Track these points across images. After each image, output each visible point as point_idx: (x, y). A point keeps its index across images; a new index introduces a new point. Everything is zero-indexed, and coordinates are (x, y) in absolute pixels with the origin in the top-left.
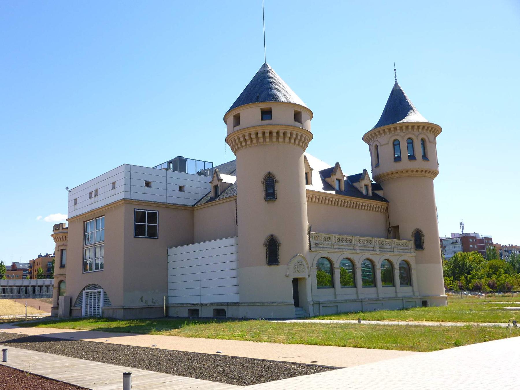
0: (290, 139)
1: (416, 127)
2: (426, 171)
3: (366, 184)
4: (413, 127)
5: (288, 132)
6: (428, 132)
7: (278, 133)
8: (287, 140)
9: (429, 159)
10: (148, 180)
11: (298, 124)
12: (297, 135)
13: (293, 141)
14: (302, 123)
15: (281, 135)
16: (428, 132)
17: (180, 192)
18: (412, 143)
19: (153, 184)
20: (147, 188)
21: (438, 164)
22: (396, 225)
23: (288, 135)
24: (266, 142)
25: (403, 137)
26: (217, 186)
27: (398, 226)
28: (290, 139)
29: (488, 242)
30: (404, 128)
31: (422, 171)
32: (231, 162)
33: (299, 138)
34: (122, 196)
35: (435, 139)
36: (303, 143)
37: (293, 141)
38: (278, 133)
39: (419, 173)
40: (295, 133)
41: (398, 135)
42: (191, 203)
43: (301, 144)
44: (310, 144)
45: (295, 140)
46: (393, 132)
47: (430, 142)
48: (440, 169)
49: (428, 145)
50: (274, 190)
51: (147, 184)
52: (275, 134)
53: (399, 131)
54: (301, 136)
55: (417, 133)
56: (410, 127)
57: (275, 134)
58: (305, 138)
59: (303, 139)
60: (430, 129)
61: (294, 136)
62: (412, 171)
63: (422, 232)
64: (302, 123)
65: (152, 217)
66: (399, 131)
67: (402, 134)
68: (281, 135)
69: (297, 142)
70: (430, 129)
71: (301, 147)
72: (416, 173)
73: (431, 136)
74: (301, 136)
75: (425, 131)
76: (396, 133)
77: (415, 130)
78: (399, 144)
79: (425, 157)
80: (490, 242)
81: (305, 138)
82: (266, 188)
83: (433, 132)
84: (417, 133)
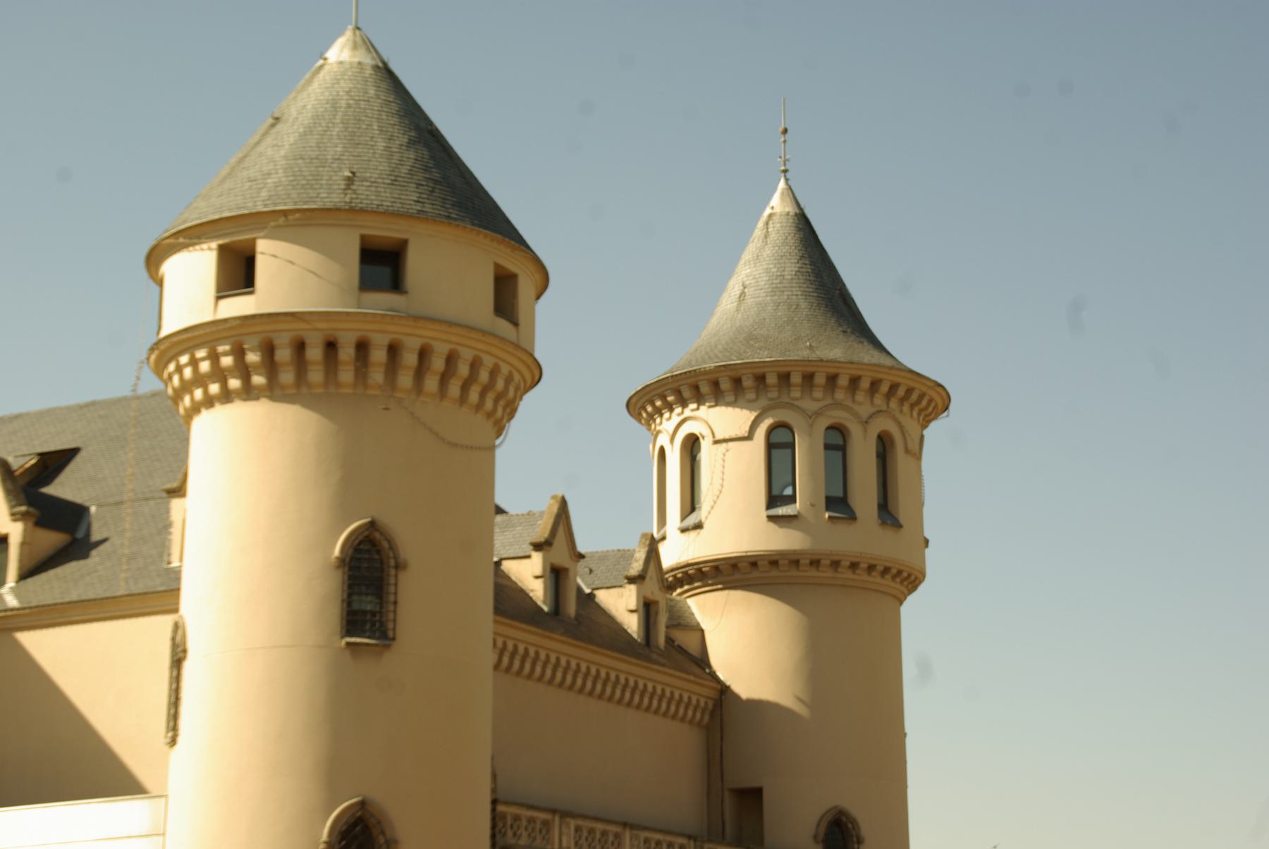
0: (445, 378)
2: (871, 568)
3: (651, 597)
4: (854, 381)
6: (906, 408)
9: (902, 520)
11: (503, 326)
12: (475, 365)
14: (516, 324)
16: (906, 408)
21: (927, 542)
22: (753, 784)
23: (438, 364)
24: (338, 385)
25: (813, 416)
28: (445, 378)
30: (820, 379)
33: (484, 376)
36: (496, 401)
40: (467, 355)
41: (790, 406)
42: (546, 534)
43: (489, 404)
44: (530, 404)
46: (773, 394)
47: (907, 451)
48: (933, 560)
49: (901, 460)
50: (349, 604)
53: (796, 393)
54: (494, 372)
55: (865, 409)
56: (843, 381)
58: (509, 380)
59: (500, 384)
60: (901, 392)
61: (463, 370)
62: (835, 564)
63: (854, 822)
64: (516, 324)
66: (796, 393)
67: (809, 405)
69: (474, 396)
70: (901, 392)
71: (490, 415)
73: (911, 424)
74: (494, 372)
76: (785, 399)
77: (860, 397)
79: (887, 512)
81: (509, 380)
83: (912, 406)
84: (865, 409)
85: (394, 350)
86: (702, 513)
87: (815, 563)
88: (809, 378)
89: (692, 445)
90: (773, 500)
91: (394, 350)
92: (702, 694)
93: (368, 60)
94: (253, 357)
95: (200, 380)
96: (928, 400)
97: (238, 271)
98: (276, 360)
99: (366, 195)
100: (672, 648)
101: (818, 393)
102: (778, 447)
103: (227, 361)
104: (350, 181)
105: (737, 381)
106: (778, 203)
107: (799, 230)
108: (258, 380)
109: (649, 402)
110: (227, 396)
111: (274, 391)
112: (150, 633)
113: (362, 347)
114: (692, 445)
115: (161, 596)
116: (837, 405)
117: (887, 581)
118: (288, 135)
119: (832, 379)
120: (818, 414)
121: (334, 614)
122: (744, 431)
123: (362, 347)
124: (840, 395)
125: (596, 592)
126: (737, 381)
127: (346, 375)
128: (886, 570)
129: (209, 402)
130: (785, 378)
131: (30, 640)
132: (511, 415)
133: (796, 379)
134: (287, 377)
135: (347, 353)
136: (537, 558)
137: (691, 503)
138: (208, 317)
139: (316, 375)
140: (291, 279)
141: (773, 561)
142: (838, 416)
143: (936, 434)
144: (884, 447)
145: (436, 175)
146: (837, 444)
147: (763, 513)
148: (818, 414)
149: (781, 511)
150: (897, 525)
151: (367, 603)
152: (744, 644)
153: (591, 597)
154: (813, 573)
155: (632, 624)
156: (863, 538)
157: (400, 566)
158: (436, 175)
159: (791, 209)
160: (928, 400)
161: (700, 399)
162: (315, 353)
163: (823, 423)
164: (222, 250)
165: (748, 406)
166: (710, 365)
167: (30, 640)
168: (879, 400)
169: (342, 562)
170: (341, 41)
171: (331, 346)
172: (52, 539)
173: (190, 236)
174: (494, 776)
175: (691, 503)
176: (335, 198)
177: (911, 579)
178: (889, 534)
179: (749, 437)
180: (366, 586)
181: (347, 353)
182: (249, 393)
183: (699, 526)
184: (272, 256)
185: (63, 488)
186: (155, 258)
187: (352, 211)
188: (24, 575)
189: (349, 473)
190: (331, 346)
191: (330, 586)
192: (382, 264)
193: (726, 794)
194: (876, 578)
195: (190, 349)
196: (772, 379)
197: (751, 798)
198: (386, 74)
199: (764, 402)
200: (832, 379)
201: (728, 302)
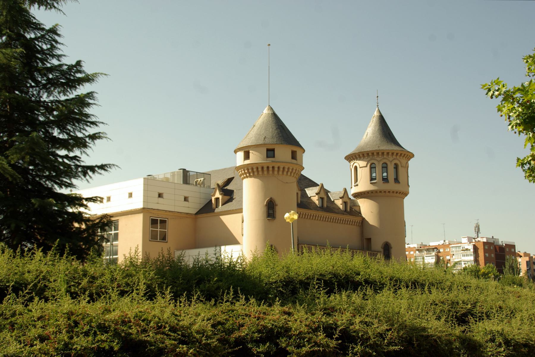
0: (287, 172)
1: (390, 154)
5: (287, 167)
7: (279, 168)
11: (294, 161)
13: (289, 174)
19: (164, 196)
20: (160, 199)
23: (286, 170)
25: (379, 161)
27: (370, 239)
28: (287, 172)
29: (510, 250)
30: (380, 154)
31: (393, 192)
33: (294, 171)
34: (140, 205)
35: (407, 162)
37: (289, 174)
38: (279, 168)
45: (291, 173)
47: (402, 167)
48: (410, 189)
49: (400, 169)
50: (274, 211)
51: (160, 195)
52: (276, 169)
53: (376, 157)
55: (391, 159)
56: (385, 154)
57: (276, 169)
61: (290, 170)
62: (385, 192)
63: (390, 244)
65: (163, 222)
66: (376, 157)
67: (378, 159)
69: (292, 175)
72: (389, 194)
73: (404, 161)
74: (296, 170)
75: (398, 157)
77: (390, 156)
79: (397, 180)
80: (513, 250)
85: (273, 167)
86: (358, 183)
87: (381, 192)
88: (378, 153)
89: (356, 168)
90: (372, 179)
91: (273, 167)
92: (358, 219)
93: (270, 112)
95: (242, 174)
96: (409, 156)
97: (247, 156)
98: (252, 171)
99: (267, 141)
100: (351, 210)
101: (380, 156)
102: (372, 168)
103: (246, 171)
104: (265, 138)
105: (363, 155)
106: (376, 114)
107: (380, 119)
108: (251, 174)
109: (350, 158)
110: (247, 177)
111: (253, 176)
112: (238, 216)
113: (268, 167)
114: (356, 168)
118: (255, 129)
120: (380, 161)
121: (265, 215)
122: (365, 165)
123: (268, 167)
124: (385, 157)
125: (335, 201)
127: (266, 173)
129: (245, 178)
131: (223, 218)
132: (408, 167)
133: (375, 154)
134: (256, 173)
135: (265, 169)
137: (356, 180)
138: (242, 164)
139: (260, 173)
140: (255, 158)
142: (385, 161)
144: (396, 167)
145: (280, 135)
146: (385, 167)
147: (369, 182)
148: (380, 161)
149: (373, 182)
150: (399, 182)
151: (271, 212)
152: (367, 209)
153: (334, 201)
154: (380, 194)
155: (341, 207)
156: (391, 186)
157: (276, 205)
159: (378, 114)
160: (409, 156)
161: (357, 159)
162: (260, 169)
163: (381, 163)
164: (245, 152)
165: (362, 160)
168: (394, 157)
169: (266, 205)
171: (263, 168)
172: (227, 198)
173: (240, 149)
174: (298, 240)
175: (356, 180)
176: (261, 142)
177: (406, 194)
178: (397, 185)
179: (366, 166)
180: (271, 210)
181: (265, 169)
183: (357, 185)
184: (252, 154)
185: (229, 187)
186: (236, 152)
187: (265, 144)
188: (222, 205)
189: (266, 189)
190: (263, 168)
192: (270, 153)
193: (365, 240)
194: (398, 194)
195: (241, 169)
196: (370, 154)
197: (369, 240)
198: (274, 115)
199: (369, 159)
200: (383, 153)
201: (365, 137)
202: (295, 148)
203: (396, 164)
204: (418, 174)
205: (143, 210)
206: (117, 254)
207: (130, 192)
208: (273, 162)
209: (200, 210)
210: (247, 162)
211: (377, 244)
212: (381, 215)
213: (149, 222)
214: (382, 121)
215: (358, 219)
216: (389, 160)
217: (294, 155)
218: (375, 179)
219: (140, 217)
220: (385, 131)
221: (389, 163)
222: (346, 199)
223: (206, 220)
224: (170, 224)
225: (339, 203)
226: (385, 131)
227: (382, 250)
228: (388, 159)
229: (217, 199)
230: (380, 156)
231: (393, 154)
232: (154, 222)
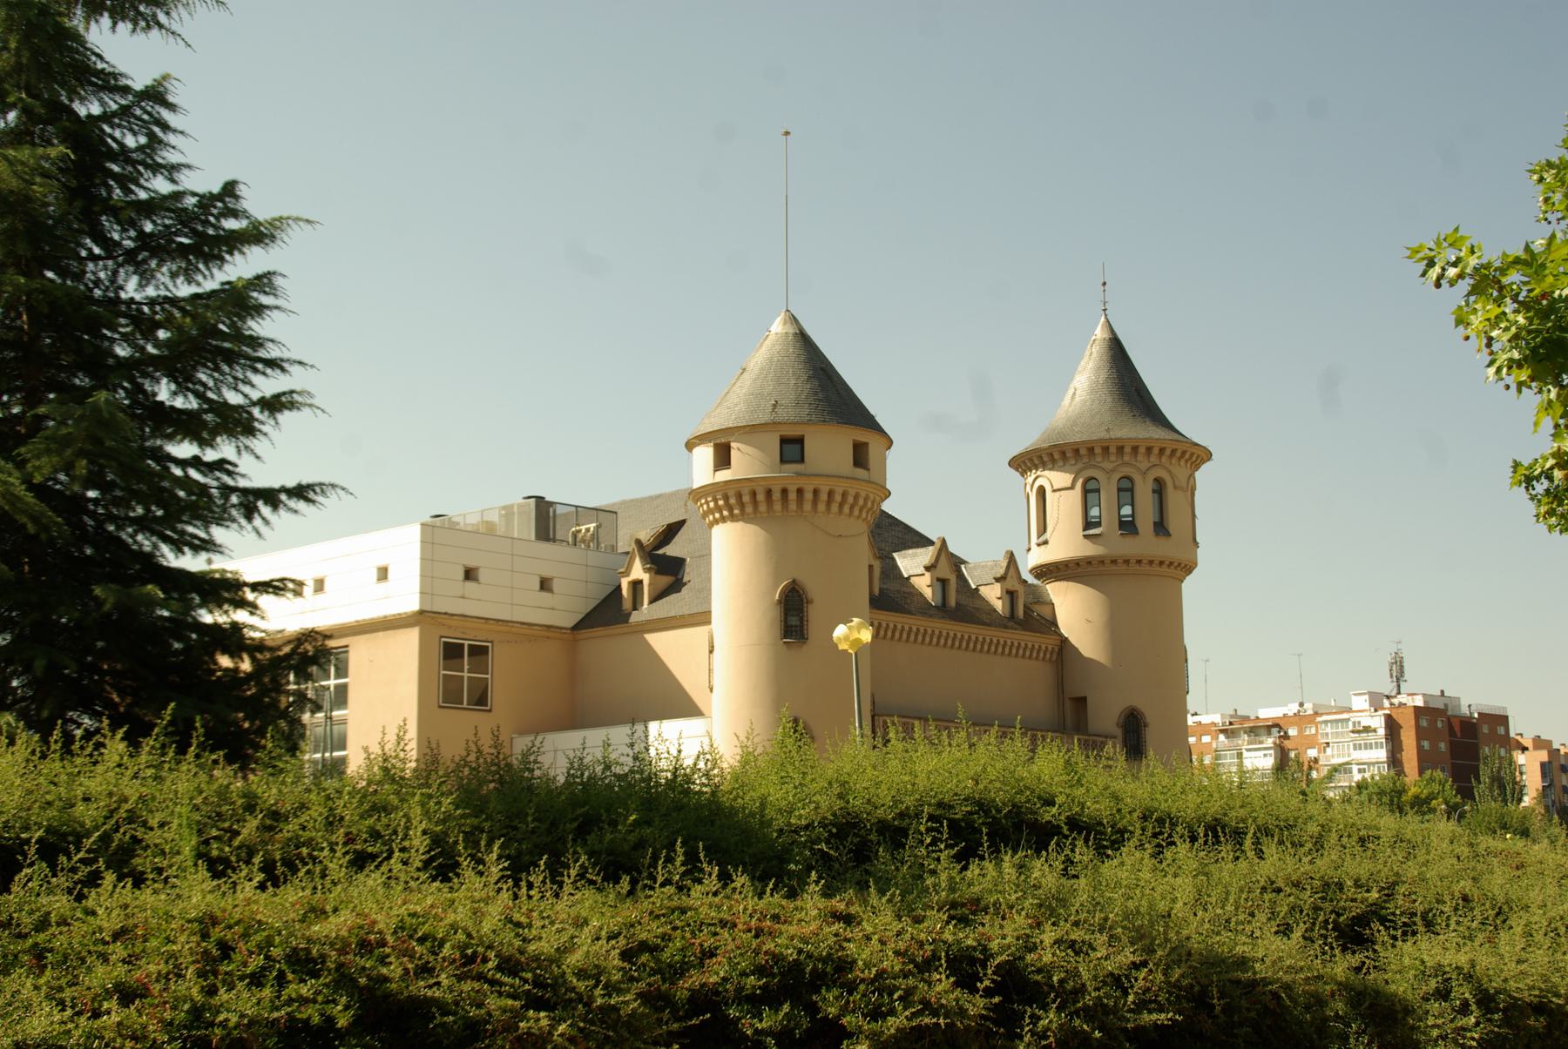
0: (841, 505)
1: (1142, 450)
3: (1011, 588)
5: (839, 491)
8: (835, 507)
10: (472, 564)
11: (860, 472)
13: (846, 509)
15: (824, 497)
17: (544, 594)
18: (1131, 490)
19: (483, 575)
20: (469, 584)
23: (838, 498)
25: (1109, 472)
26: (641, 582)
28: (841, 505)
29: (1493, 730)
30: (1113, 450)
31: (1151, 562)
32: (652, 498)
33: (861, 502)
34: (412, 604)
35: (1192, 475)
38: (816, 492)
39: (1146, 568)
41: (1094, 466)
45: (852, 508)
47: (1175, 487)
49: (1173, 498)
50: (801, 619)
51: (470, 574)
52: (809, 496)
55: (1144, 465)
56: (1128, 450)
57: (809, 496)
62: (1127, 562)
65: (479, 652)
67: (1107, 465)
68: (824, 497)
69: (856, 512)
73: (1181, 471)
75: (1164, 459)
77: (1140, 458)
78: (1098, 491)
79: (1161, 528)
80: (1501, 730)
82: (786, 615)
85: (800, 491)
87: (1114, 562)
88: (1106, 450)
89: (1042, 492)
90: (1088, 525)
91: (800, 491)
92: (1048, 642)
94: (732, 501)
96: (1197, 455)
97: (723, 459)
98: (739, 501)
100: (1029, 614)
101: (1113, 458)
104: (775, 406)
105: (1063, 453)
106: (1100, 333)
107: (1111, 348)
108: (736, 512)
109: (1025, 462)
110: (723, 519)
111: (743, 517)
113: (784, 492)
114: (1042, 492)
115: (703, 618)
116: (1126, 464)
117: (1172, 570)
118: (748, 378)
119: (1120, 449)
120: (1113, 470)
121: (777, 631)
123: (784, 492)
124: (1126, 458)
126: (1063, 453)
127: (778, 507)
128: (1171, 563)
130: (1091, 450)
133: (1098, 450)
134: (749, 509)
135: (777, 495)
136: (928, 575)
137: (1043, 529)
139: (763, 508)
140: (746, 463)
141: (1089, 561)
142: (1127, 471)
143: (1203, 475)
144: (1159, 489)
146: (1126, 490)
148: (1113, 470)
150: (1167, 534)
151: (794, 621)
152: (1074, 612)
153: (977, 590)
154: (1113, 567)
155: (998, 605)
156: (1146, 544)
158: (820, 396)
159: (1107, 335)
160: (1197, 455)
161: (1044, 466)
162: (761, 497)
163: (1117, 476)
166: (1045, 445)
167: (651, 638)
168: (1153, 459)
169: (780, 602)
170: (779, 319)
171: (769, 493)
172: (665, 580)
173: (701, 439)
175: (1043, 529)
177: (1188, 568)
178: (1162, 541)
179: (1072, 488)
181: (777, 495)
182: (733, 518)
183: (1046, 543)
185: (671, 550)
186: (690, 446)
188: (651, 602)
189: (778, 554)
190: (769, 493)
191: (775, 614)
192: (792, 448)
194: (1164, 569)
198: (804, 340)
199: (1080, 465)
200: (1120, 449)
202: (862, 435)
203: (1157, 480)
204: (1223, 508)
205: (421, 618)
206: (343, 747)
207: (382, 563)
208: (799, 474)
209: (588, 614)
210: (724, 475)
211: (1105, 716)
212: (1116, 628)
213: (437, 653)
214: (1117, 353)
215: (1048, 642)
216: (1138, 469)
217: (860, 456)
218: (1098, 524)
219: (411, 639)
220: (1126, 384)
221: (1137, 478)
222: (1012, 584)
223: (603, 646)
224: (500, 659)
225: (993, 595)
226: (1126, 384)
227: (1119, 732)
228: (1134, 466)
229: (637, 584)
230: (1113, 458)
231: (1149, 450)
232: (452, 652)
